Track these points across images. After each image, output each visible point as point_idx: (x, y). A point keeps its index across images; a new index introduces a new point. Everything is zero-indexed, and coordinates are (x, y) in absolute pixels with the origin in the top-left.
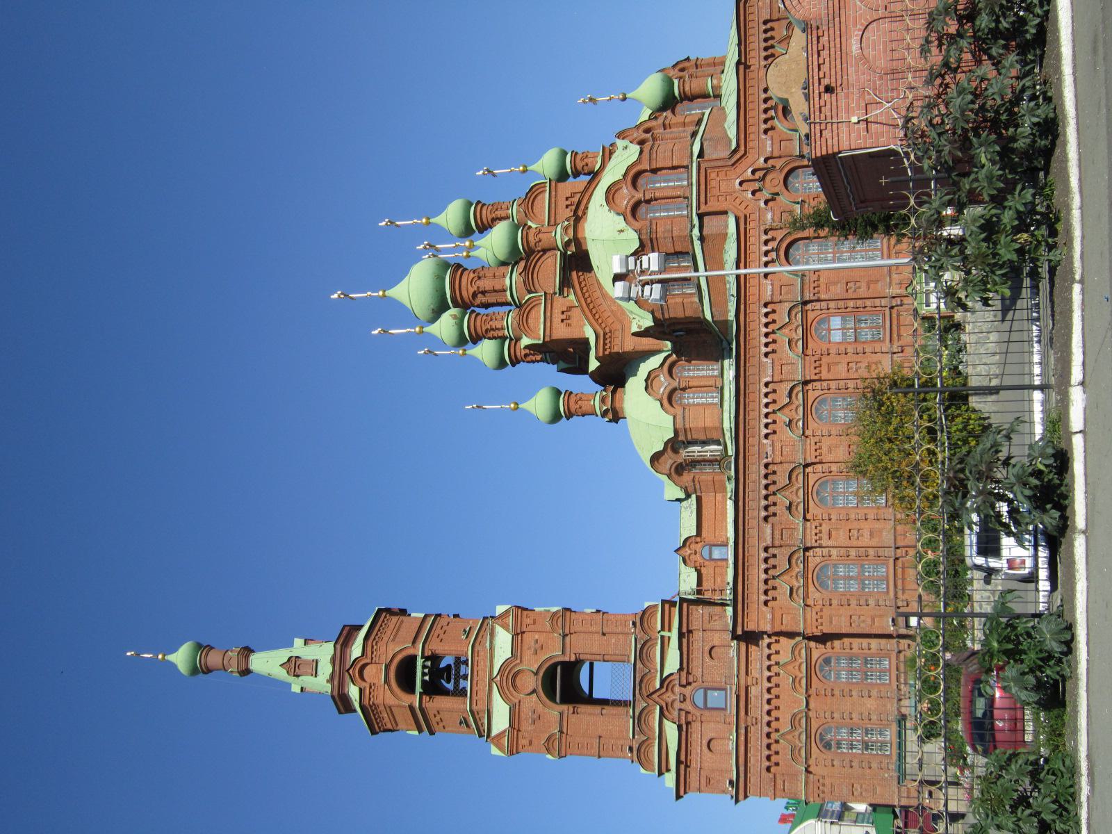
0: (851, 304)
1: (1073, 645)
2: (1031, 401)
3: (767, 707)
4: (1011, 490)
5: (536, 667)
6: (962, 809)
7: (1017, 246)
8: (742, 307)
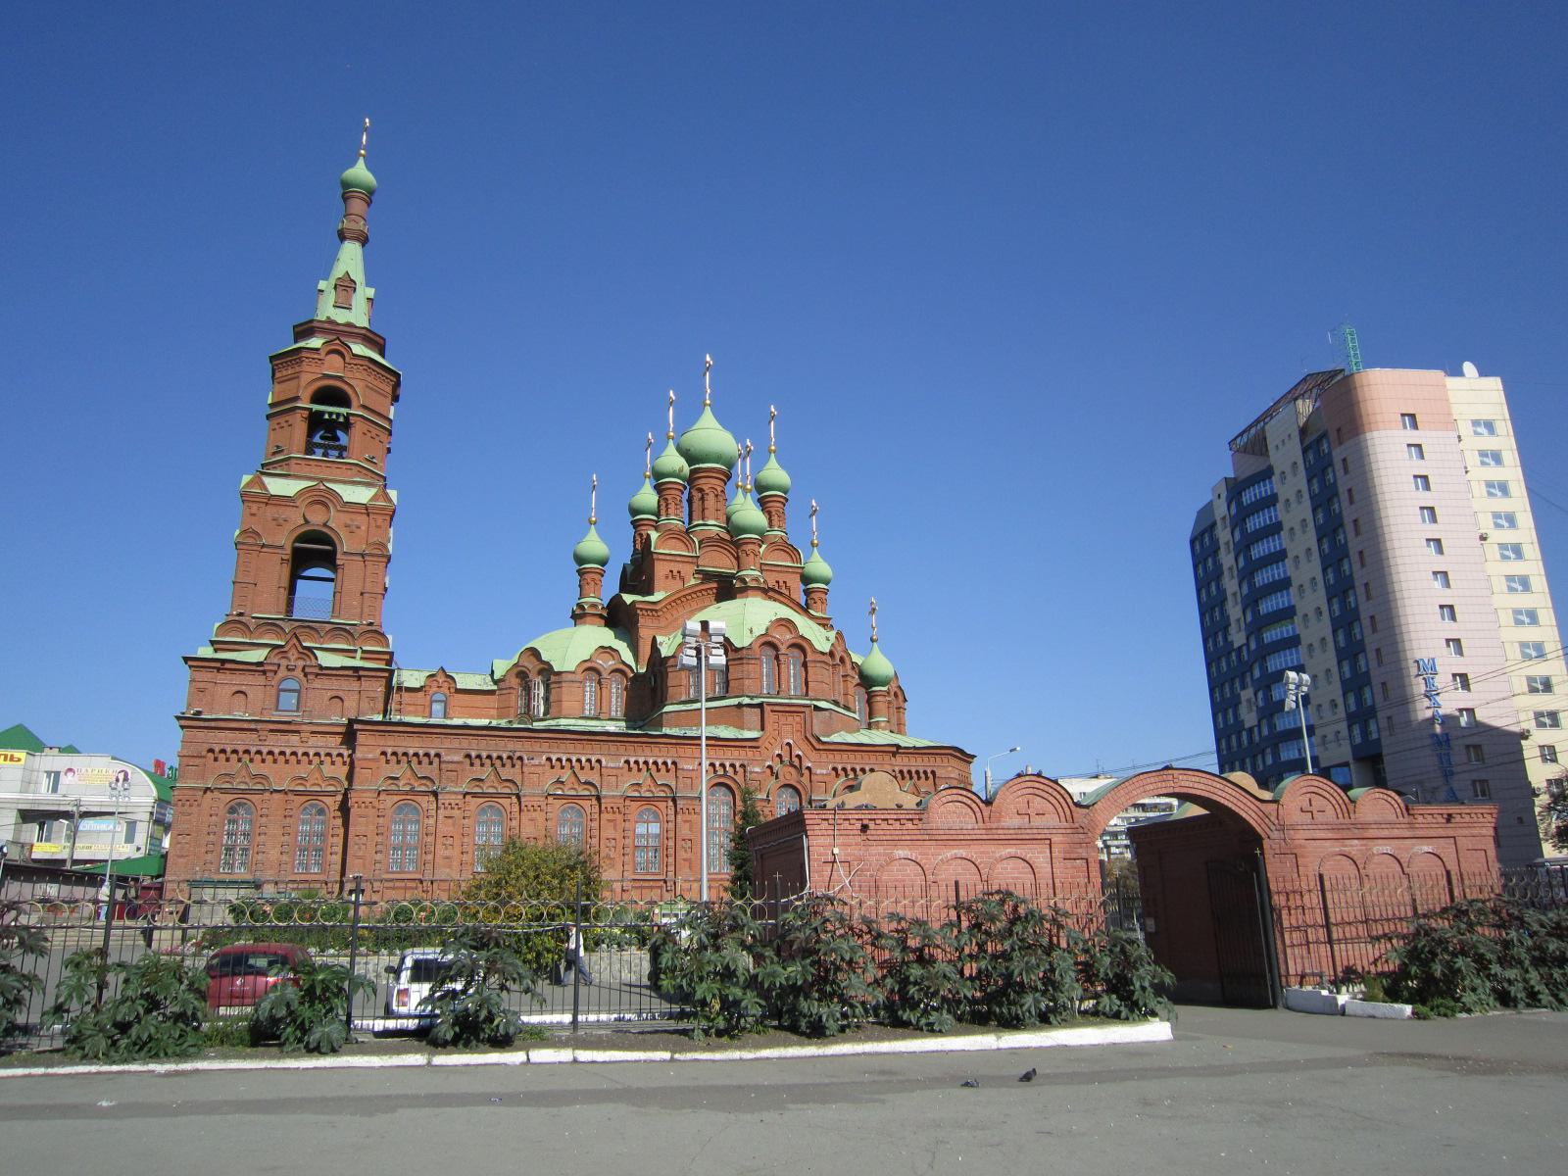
0: (671, 843)
1: (316, 1053)
2: (563, 1012)
3: (276, 751)
4: (477, 992)
5: (333, 525)
6: (155, 945)
7: (708, 1000)
8: (674, 741)
